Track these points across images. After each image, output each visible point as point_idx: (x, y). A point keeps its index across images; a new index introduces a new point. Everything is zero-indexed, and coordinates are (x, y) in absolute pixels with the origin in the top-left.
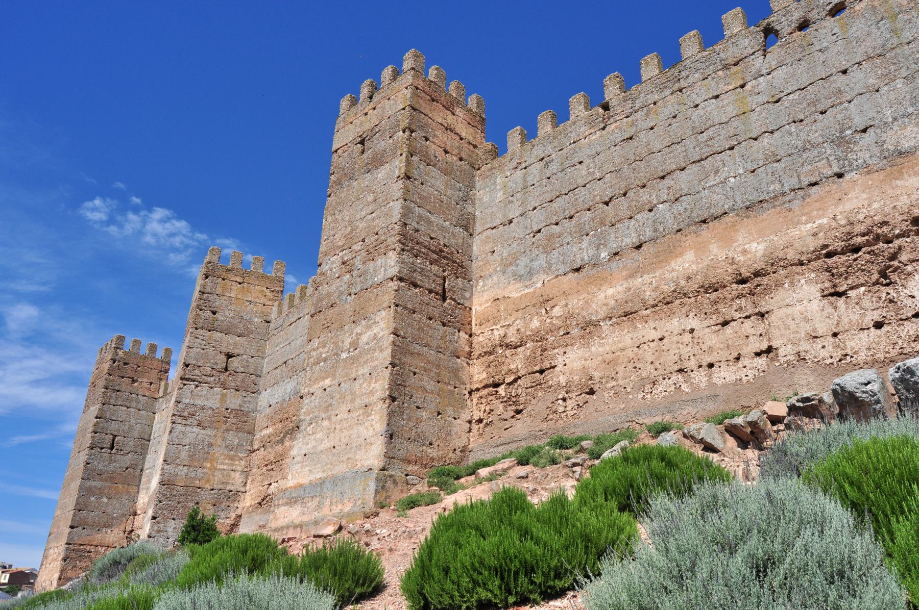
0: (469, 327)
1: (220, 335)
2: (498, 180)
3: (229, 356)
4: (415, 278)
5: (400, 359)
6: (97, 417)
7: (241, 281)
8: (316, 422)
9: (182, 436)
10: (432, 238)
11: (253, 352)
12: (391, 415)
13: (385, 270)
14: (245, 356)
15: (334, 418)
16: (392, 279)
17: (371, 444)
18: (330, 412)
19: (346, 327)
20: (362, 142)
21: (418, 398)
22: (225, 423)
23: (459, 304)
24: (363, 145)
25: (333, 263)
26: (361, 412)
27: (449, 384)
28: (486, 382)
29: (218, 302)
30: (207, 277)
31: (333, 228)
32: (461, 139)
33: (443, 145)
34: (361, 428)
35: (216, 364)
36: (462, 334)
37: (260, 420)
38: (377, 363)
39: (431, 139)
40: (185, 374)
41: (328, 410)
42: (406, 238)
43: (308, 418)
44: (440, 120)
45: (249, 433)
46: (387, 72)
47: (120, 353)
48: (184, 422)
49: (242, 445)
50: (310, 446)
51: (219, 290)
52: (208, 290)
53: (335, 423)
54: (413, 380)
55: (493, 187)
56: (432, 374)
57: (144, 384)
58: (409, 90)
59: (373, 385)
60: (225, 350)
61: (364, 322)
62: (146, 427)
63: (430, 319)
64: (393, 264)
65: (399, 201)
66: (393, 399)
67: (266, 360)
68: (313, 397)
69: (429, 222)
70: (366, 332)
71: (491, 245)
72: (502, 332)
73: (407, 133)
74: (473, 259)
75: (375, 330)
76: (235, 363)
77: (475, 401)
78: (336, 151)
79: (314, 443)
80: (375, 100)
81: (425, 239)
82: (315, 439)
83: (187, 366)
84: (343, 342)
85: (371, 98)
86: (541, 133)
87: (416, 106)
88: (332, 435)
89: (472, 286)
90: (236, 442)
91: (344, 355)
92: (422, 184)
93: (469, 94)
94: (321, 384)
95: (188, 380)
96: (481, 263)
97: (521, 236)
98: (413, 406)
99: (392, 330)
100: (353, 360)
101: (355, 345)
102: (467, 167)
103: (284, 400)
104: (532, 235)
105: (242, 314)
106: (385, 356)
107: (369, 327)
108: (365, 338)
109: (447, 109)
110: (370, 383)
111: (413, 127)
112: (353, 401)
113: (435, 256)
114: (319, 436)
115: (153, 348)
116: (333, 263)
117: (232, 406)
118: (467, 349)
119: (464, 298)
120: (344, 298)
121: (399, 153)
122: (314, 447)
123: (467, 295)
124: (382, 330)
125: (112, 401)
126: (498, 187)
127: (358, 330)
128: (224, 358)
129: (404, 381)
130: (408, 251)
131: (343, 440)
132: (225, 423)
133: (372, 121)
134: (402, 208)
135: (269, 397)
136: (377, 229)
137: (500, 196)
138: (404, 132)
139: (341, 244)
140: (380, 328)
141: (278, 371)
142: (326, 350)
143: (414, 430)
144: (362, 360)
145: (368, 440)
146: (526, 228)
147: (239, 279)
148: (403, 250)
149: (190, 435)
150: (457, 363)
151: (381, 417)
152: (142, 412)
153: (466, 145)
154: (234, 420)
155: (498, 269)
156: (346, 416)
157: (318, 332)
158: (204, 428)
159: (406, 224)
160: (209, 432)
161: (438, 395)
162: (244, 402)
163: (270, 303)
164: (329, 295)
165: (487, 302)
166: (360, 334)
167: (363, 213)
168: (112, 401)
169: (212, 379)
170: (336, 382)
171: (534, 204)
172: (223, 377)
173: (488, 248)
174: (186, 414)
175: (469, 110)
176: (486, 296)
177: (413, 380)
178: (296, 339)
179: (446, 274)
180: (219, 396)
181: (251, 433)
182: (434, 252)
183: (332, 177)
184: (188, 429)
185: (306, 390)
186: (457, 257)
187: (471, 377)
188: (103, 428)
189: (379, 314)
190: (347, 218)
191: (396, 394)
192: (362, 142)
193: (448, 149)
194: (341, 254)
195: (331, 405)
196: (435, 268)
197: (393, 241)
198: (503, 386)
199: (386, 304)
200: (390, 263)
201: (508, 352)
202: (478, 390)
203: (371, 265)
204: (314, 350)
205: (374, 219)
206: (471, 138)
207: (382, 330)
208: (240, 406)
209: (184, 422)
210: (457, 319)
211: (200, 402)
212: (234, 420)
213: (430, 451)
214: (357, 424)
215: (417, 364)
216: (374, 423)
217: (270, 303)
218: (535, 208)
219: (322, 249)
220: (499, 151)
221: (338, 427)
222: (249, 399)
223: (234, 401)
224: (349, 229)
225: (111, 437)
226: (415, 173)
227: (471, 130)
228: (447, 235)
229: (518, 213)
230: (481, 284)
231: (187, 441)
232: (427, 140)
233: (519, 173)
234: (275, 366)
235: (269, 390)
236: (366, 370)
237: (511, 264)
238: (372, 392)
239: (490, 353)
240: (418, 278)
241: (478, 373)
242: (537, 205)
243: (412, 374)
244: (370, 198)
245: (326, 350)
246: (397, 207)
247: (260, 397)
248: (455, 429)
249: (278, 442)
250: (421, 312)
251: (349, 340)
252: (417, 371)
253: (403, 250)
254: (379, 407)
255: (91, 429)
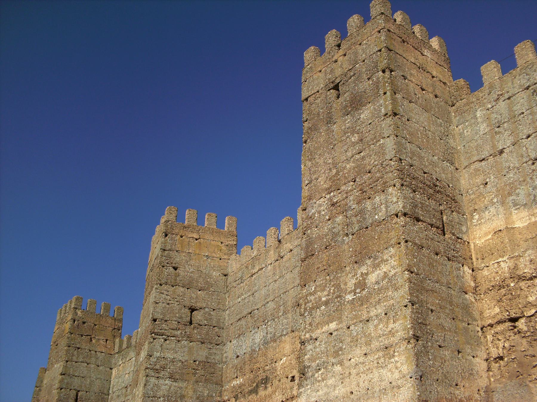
0: (470, 261)
1: (182, 289)
2: (478, 114)
3: (192, 310)
4: (418, 213)
5: (417, 297)
6: (61, 374)
7: (197, 237)
8: (326, 368)
9: (156, 388)
10: (425, 173)
11: (214, 305)
12: (418, 356)
13: (387, 207)
14: (207, 310)
15: (347, 363)
16: (397, 216)
17: (399, 387)
18: (342, 357)
19: (348, 269)
20: (336, 88)
21: (438, 335)
22: (195, 374)
23: (458, 238)
24: (338, 90)
25: (320, 205)
26: (381, 354)
27: (463, 321)
28: (499, 317)
29: (178, 258)
30: (166, 235)
31: (315, 172)
32: (433, 77)
33: (419, 83)
34: (384, 372)
35: (181, 318)
36: (466, 268)
37: (229, 372)
38: (392, 302)
39: (408, 77)
40: (154, 328)
41: (338, 355)
42: (403, 174)
43: (314, 365)
44: (413, 60)
45: (217, 384)
46: (354, 21)
47: (79, 312)
48: (157, 375)
49: (212, 396)
50: (320, 393)
51: (178, 247)
52: (168, 248)
53: (349, 367)
54: (432, 317)
55: (473, 121)
56: (447, 311)
57: (101, 342)
58: (383, 33)
59: (391, 326)
60: (188, 304)
61: (369, 262)
62: (105, 382)
63: (437, 254)
64: (395, 200)
65: (391, 138)
66: (417, 338)
67: (227, 312)
68: (318, 343)
69: (421, 158)
70: (373, 272)
71: (482, 177)
72: (511, 264)
73: (388, 72)
74: (464, 192)
75: (384, 268)
76: (198, 316)
77: (489, 338)
78: (306, 99)
79: (325, 390)
80: (343, 47)
81: (419, 174)
82: (326, 385)
83: (155, 320)
84: (346, 284)
85: (339, 46)
86: (520, 62)
87: (391, 47)
88: (347, 380)
89: (466, 220)
90: (206, 393)
91: (349, 297)
92: (408, 120)
93: (430, 38)
94: (325, 328)
95: (157, 334)
96: (473, 196)
97: (517, 165)
98: (436, 345)
99: (405, 266)
100: (363, 301)
101: (361, 285)
102: (443, 103)
103: (254, 350)
104: (530, 162)
105: (201, 269)
106: (401, 294)
107: (376, 266)
108: (372, 278)
109: (416, 49)
110: (387, 323)
111: (392, 67)
112: (368, 343)
113: (431, 191)
114: (331, 382)
115: (107, 308)
116: (320, 205)
117: (200, 359)
118: (473, 284)
119: (461, 231)
120: (340, 239)
121: (381, 92)
122: (327, 394)
123: (464, 229)
124: (393, 267)
125: (75, 358)
126: (479, 120)
127: (364, 269)
128: (188, 311)
129: (424, 320)
130: (407, 186)
131: (361, 384)
132: (195, 374)
133: (344, 66)
134: (395, 144)
135: (234, 349)
136: (368, 168)
137: (483, 128)
138: (384, 71)
139: (326, 186)
140: (391, 264)
141: (243, 322)
142: (326, 293)
143: (441, 371)
144: (372, 300)
145: (394, 384)
146: (522, 156)
147: (195, 236)
148: (402, 185)
149: (163, 387)
150: (466, 299)
151: (407, 358)
152: (101, 368)
153: (438, 83)
154: (202, 372)
155: (495, 200)
156: (362, 359)
157: (314, 277)
158: (176, 380)
159: (401, 160)
160: (181, 384)
161: (456, 332)
162: (211, 354)
163: (226, 257)
164: (320, 238)
165: (486, 234)
166: (367, 274)
167: (349, 154)
168: (75, 358)
169: (179, 332)
170: (344, 325)
171: (526, 132)
172: (188, 330)
173: (479, 180)
174: (158, 367)
175: (434, 51)
176: (485, 228)
177: (432, 317)
178: (259, 289)
179: (441, 208)
180: (186, 349)
181: (220, 383)
182: (429, 186)
183: (306, 124)
184: (161, 381)
185: (308, 336)
186: (449, 191)
187: (481, 313)
188: (67, 383)
189: (386, 251)
190: (330, 161)
191: (419, 333)
192: (336, 88)
193: (424, 87)
194: (328, 196)
195: (341, 349)
196: (432, 203)
197: (392, 176)
198: (523, 320)
199: (393, 241)
200: (395, 199)
201: (522, 284)
202: (491, 326)
203: (368, 204)
204: (311, 294)
205: (363, 158)
206: (441, 76)
207: (393, 267)
208: (207, 358)
209: (157, 375)
210: (457, 253)
211: (169, 355)
212: (202, 372)
213: (457, 392)
214: (377, 367)
215: (432, 301)
216: (399, 365)
217: (226, 257)
218: (528, 137)
219: (305, 192)
220: (476, 83)
221: (354, 372)
222: (214, 351)
223: (202, 353)
224: (334, 171)
225: (75, 392)
226: (401, 110)
227: (440, 68)
228: (438, 170)
229: (508, 143)
230: (477, 217)
231: (160, 393)
232: (405, 78)
233: (502, 105)
234: (238, 317)
235: (235, 342)
236: (380, 310)
237: (510, 194)
238: (392, 333)
239: (501, 287)
240: (420, 213)
241: (491, 309)
242: (530, 132)
243: (430, 312)
244: (355, 138)
245: (326, 293)
246: (390, 144)
247: (225, 348)
248: (476, 368)
249: (250, 392)
250: (428, 248)
251: (354, 281)
252: (434, 308)
253: (402, 185)
254: (403, 348)
255: (57, 386)
